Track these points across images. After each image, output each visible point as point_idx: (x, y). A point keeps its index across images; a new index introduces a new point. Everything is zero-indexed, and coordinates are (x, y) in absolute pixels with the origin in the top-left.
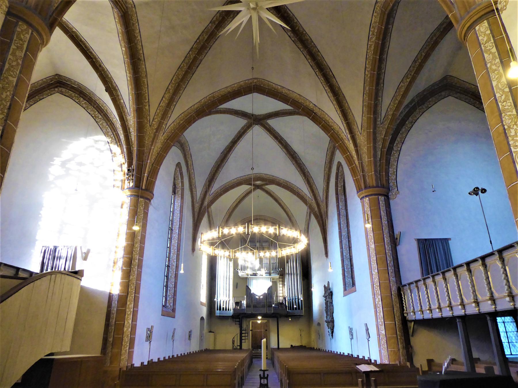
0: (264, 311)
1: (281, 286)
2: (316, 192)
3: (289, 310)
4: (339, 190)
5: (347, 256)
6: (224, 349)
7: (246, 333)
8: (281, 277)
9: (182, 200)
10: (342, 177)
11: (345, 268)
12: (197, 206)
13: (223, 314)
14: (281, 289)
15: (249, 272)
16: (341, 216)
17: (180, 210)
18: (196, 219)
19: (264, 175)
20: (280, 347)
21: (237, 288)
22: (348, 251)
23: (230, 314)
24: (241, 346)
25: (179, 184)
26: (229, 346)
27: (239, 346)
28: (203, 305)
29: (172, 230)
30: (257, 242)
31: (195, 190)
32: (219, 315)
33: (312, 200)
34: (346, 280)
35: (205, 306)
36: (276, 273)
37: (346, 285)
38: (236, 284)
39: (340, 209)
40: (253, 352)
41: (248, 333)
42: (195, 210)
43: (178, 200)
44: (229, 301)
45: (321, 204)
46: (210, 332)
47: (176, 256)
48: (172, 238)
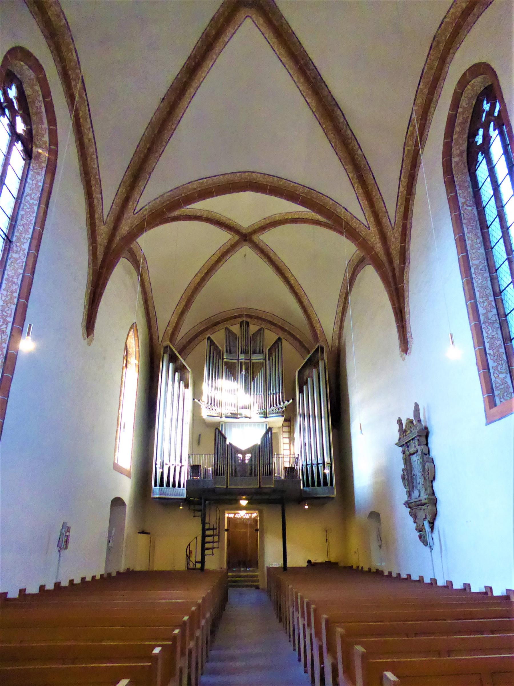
0: (253, 484)
1: (287, 441)
2: (379, 205)
3: (304, 486)
4: (453, 165)
5: (490, 315)
6: (168, 569)
7: (216, 535)
8: (287, 424)
9: (49, 176)
10: (462, 130)
11: (487, 346)
12: (103, 230)
13: (166, 495)
14: (287, 447)
15: (227, 410)
16: (464, 221)
17: (40, 197)
18: (100, 257)
19: (259, 175)
20: (289, 564)
21: (199, 443)
22: (493, 303)
23: (183, 495)
24: (203, 562)
25: (43, 136)
26: (181, 565)
27: (198, 562)
28: (122, 473)
29: (11, 242)
30: (241, 353)
31: (98, 190)
32: (157, 496)
33: (369, 228)
34: (493, 379)
35: (129, 476)
36: (278, 413)
37: (493, 393)
38: (198, 436)
39: (461, 205)
40: (230, 574)
41: (219, 536)
42: (99, 239)
43: (38, 174)
44: (181, 467)
45: (389, 233)
46: (143, 532)
47: (14, 307)
48: (9, 262)
